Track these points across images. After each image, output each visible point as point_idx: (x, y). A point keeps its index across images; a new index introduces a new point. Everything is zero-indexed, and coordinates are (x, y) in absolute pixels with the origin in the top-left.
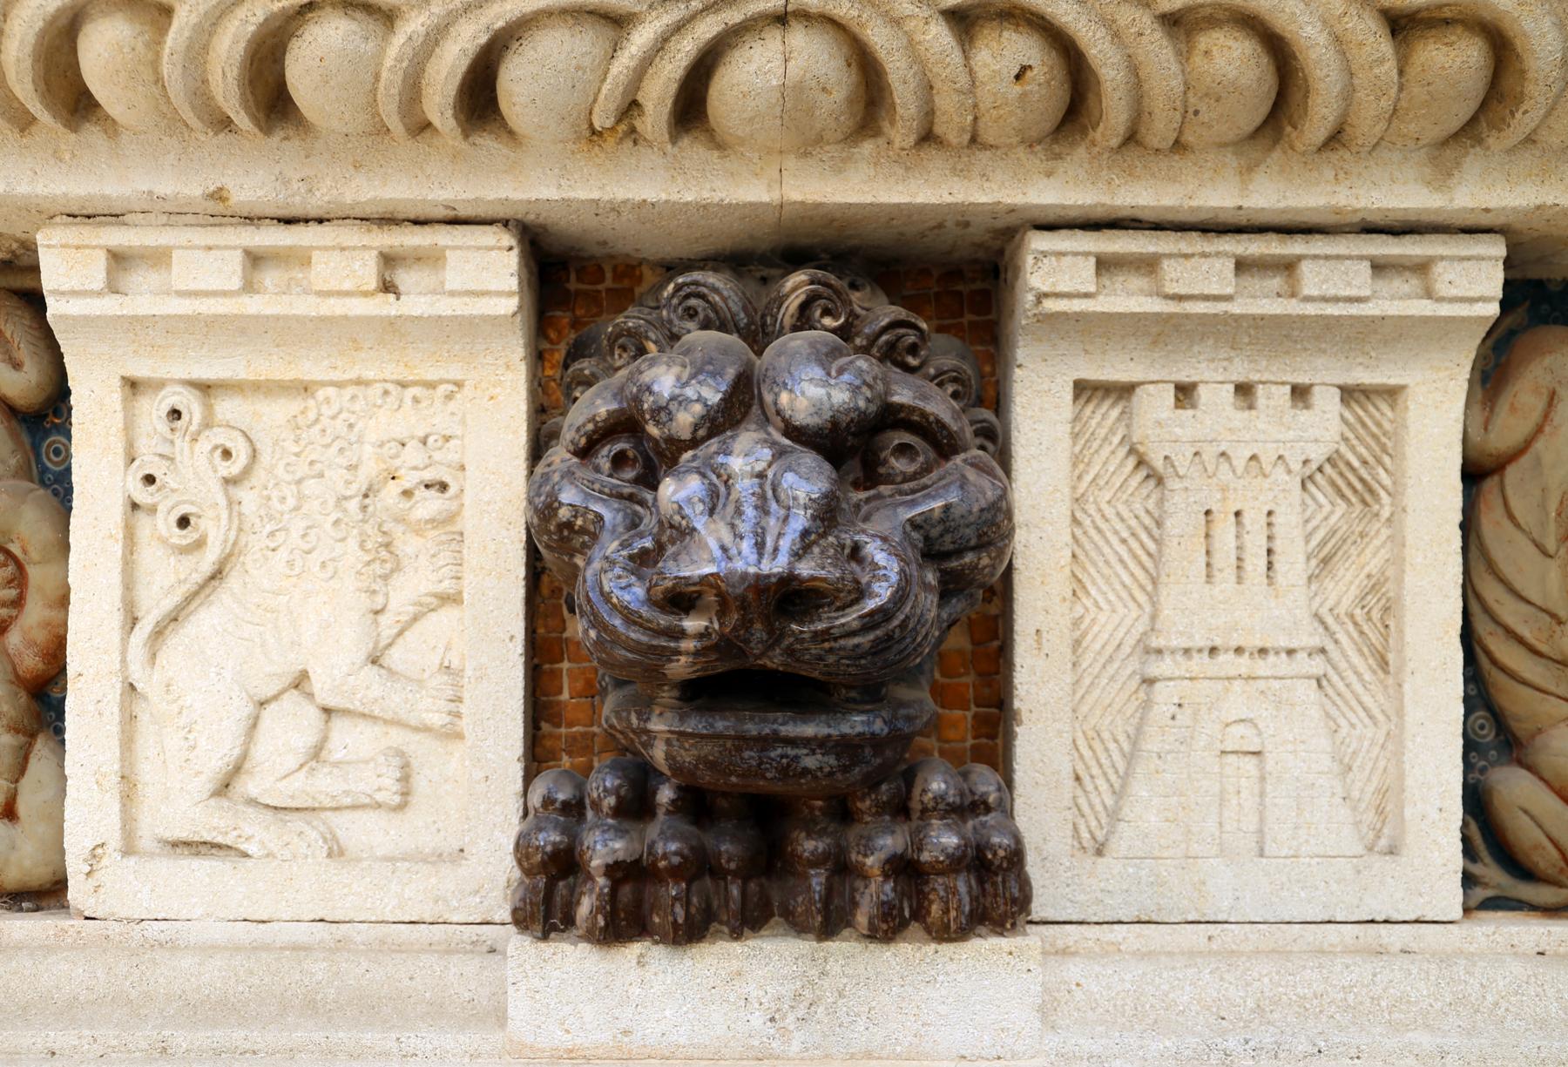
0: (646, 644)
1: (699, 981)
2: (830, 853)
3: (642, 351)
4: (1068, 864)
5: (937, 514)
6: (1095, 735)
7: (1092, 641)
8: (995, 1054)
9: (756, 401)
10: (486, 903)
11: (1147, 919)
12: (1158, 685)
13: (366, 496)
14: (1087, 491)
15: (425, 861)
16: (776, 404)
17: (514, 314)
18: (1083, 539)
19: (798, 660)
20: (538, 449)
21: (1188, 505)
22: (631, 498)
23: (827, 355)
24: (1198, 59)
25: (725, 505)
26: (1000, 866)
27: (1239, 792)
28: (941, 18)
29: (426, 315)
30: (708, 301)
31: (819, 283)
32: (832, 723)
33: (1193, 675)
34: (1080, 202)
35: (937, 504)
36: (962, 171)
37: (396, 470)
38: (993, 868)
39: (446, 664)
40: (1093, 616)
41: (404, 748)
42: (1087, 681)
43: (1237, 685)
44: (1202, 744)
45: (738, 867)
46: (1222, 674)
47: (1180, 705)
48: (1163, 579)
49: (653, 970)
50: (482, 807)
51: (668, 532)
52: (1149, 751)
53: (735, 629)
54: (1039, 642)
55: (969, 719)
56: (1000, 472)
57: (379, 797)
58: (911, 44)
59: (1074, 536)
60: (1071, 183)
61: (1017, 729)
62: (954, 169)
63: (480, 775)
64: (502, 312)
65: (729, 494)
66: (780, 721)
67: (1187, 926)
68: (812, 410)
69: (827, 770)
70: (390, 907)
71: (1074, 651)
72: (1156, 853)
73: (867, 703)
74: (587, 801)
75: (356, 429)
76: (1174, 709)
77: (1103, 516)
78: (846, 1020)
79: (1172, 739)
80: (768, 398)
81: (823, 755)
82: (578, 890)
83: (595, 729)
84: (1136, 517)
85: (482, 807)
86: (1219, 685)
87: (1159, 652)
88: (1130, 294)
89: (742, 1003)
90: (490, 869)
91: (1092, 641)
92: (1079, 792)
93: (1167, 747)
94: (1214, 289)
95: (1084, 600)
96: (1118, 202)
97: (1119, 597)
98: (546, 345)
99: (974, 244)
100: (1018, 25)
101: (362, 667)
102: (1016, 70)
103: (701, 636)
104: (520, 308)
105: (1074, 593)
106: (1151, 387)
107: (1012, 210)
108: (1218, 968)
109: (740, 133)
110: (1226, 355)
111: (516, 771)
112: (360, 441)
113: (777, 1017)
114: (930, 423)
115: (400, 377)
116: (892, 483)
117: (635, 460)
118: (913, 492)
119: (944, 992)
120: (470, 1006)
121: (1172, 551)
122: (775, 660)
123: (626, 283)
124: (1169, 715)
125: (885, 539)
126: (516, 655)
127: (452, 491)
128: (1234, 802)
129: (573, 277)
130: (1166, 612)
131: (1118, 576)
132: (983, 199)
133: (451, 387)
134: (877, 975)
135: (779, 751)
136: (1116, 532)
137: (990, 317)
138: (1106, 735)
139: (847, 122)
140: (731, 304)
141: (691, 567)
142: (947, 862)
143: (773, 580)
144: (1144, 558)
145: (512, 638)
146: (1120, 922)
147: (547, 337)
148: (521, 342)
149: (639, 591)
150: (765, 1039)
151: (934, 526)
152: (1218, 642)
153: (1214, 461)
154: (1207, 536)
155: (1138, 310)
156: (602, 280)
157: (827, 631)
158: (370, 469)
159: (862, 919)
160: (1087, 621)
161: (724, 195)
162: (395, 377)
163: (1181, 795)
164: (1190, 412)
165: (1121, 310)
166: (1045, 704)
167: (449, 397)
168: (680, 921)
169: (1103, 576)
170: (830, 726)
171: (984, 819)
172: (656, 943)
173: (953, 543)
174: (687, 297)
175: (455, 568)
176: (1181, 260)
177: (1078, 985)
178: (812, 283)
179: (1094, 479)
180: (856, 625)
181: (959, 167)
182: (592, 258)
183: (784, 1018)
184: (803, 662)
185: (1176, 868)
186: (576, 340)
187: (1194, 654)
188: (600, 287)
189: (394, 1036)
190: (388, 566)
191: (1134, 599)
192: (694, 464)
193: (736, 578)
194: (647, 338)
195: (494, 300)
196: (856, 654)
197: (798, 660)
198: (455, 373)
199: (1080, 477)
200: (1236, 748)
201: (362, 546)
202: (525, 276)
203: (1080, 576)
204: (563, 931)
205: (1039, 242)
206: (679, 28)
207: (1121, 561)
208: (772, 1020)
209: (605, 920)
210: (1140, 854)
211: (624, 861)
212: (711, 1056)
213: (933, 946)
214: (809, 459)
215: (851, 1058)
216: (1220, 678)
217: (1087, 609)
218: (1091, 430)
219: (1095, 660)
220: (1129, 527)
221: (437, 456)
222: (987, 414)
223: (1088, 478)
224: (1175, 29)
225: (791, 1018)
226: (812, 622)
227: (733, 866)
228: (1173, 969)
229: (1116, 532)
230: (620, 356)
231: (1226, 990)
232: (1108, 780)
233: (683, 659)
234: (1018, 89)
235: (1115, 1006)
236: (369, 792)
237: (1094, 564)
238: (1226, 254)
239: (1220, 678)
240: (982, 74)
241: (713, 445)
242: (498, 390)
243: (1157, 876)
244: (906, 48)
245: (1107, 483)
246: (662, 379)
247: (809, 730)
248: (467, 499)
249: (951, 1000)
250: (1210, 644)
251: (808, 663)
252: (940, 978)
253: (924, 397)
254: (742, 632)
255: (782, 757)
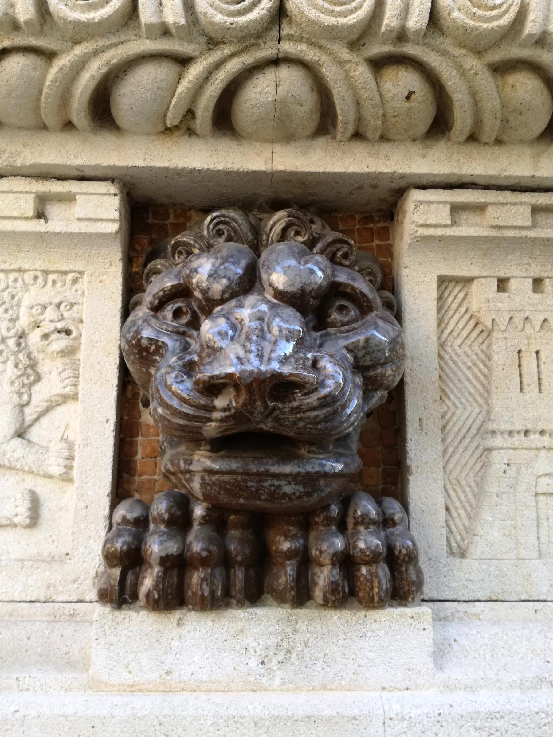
0: (192, 415)
1: (216, 636)
2: (299, 550)
3: (189, 253)
4: (444, 562)
5: (361, 343)
6: (457, 483)
7: (453, 426)
8: (404, 686)
9: (258, 280)
10: (81, 588)
11: (496, 598)
12: (494, 453)
13: (21, 337)
14: (446, 339)
15: (43, 561)
16: (269, 279)
17: (117, 233)
18: (445, 367)
19: (281, 425)
20: (126, 312)
21: (507, 347)
22: (184, 334)
23: (298, 254)
24: (508, 90)
25: (240, 335)
26: (403, 560)
27: (548, 519)
28: (364, 63)
29: (63, 232)
30: (231, 226)
31: (293, 217)
32: (301, 465)
33: (516, 446)
34: (441, 172)
35: (361, 338)
36: (374, 154)
37: (41, 322)
38: (399, 561)
39: (65, 437)
40: (453, 411)
41: (35, 489)
42: (450, 450)
43: (543, 453)
44: (523, 488)
45: (242, 560)
46: (533, 446)
47: (508, 465)
48: (494, 389)
49: (187, 629)
50: (82, 526)
51: (206, 351)
52: (490, 492)
53: (244, 405)
54: (421, 426)
55: (380, 472)
56: (396, 322)
57: (16, 520)
58: (348, 77)
59: (440, 365)
60: (436, 161)
61: (410, 478)
62: (369, 153)
63: (83, 505)
64: (110, 231)
65: (242, 329)
66: (270, 463)
67: (521, 603)
68: (290, 283)
69: (298, 494)
70: (18, 592)
71: (442, 432)
72: (499, 556)
73: (321, 454)
74: (150, 518)
75: (16, 298)
76: (505, 467)
77: (456, 354)
78: (309, 663)
79: (505, 485)
80: (264, 276)
81: (295, 485)
82: (141, 576)
83: (156, 477)
84: (476, 354)
85: (82, 526)
86: (532, 453)
87: (493, 432)
88: (470, 226)
89: (244, 651)
90: (85, 565)
91: (453, 426)
92: (449, 518)
93: (502, 490)
94: (520, 223)
95: (447, 402)
96: (463, 172)
97: (467, 400)
98: (133, 254)
99: (380, 199)
100: (407, 68)
101: (11, 439)
102: (406, 94)
103: (225, 410)
104: (120, 228)
105: (441, 398)
106: (483, 280)
107: (403, 176)
108: (543, 629)
109: (250, 130)
110: (527, 262)
111: (106, 502)
112: (19, 305)
113: (266, 660)
114: (357, 294)
115: (45, 268)
116: (335, 327)
117: (186, 313)
118: (348, 331)
119: (371, 644)
120: (67, 657)
121: (497, 373)
122: (268, 426)
123: (182, 220)
124: (503, 471)
125: (331, 356)
126: (110, 431)
127: (74, 334)
128: (546, 524)
129: (151, 216)
130: (497, 409)
131: (466, 388)
132: (386, 170)
133: (76, 275)
134: (329, 631)
135: (269, 482)
136: (464, 363)
137: (388, 242)
138: (463, 483)
139: (312, 125)
140: (243, 227)
141: (221, 369)
142: (371, 556)
143: (268, 376)
144: (482, 378)
145: (108, 421)
146: (479, 601)
147: (135, 250)
148: (120, 249)
149: (189, 384)
150: (258, 677)
151: (359, 350)
152: (530, 427)
153: (522, 322)
154: (520, 366)
155: (475, 234)
156: (168, 218)
157: (299, 407)
158: (24, 322)
159: (318, 594)
160: (449, 414)
161: (240, 166)
162: (42, 268)
163: (512, 519)
164: (506, 294)
165: (465, 234)
166: (426, 463)
167: (75, 281)
168: (206, 594)
169: (457, 388)
170: (299, 467)
171: (391, 530)
172: (190, 610)
173: (371, 361)
174: (218, 224)
175: (74, 380)
176: (500, 207)
177: (455, 641)
178: (289, 216)
179: (451, 333)
180: (316, 403)
181: (373, 152)
182: (162, 205)
183: (270, 661)
184: (284, 426)
185: (512, 565)
186: (152, 251)
187: (516, 434)
188: (166, 222)
189: (15, 676)
190: (32, 378)
191: (476, 401)
192: (222, 313)
193: (247, 374)
194: (194, 247)
195: (105, 224)
196: (315, 421)
197: (281, 425)
198: (79, 266)
199: (442, 332)
200: (545, 491)
201: (16, 366)
202: (124, 212)
203: (444, 388)
204: (131, 603)
205: (416, 195)
206: (218, 65)
207: (468, 379)
208: (263, 663)
209: (158, 594)
210: (489, 556)
211: (172, 555)
212: (223, 689)
213: (363, 612)
214: (289, 311)
215: (313, 689)
216: (532, 449)
217: (449, 408)
218: (448, 305)
219: (455, 437)
220: (472, 361)
221: (66, 314)
222: (387, 294)
223: (447, 332)
224: (495, 73)
225: (274, 661)
226: (290, 401)
227: (239, 558)
228: (515, 630)
229: (464, 363)
230: (179, 257)
231: (549, 643)
232: (466, 511)
233: (213, 424)
234: (407, 105)
235: (479, 655)
236: (10, 517)
237: (452, 381)
238: (525, 203)
239: (532, 449)
240: (388, 96)
241: (233, 303)
242: (105, 277)
243: (501, 571)
244: (345, 80)
245: (458, 335)
246: (204, 266)
247: (287, 469)
248: (83, 340)
249: (376, 649)
250: (524, 428)
251: (287, 426)
252: (369, 634)
253: (353, 279)
254: (249, 407)
255: (271, 485)
